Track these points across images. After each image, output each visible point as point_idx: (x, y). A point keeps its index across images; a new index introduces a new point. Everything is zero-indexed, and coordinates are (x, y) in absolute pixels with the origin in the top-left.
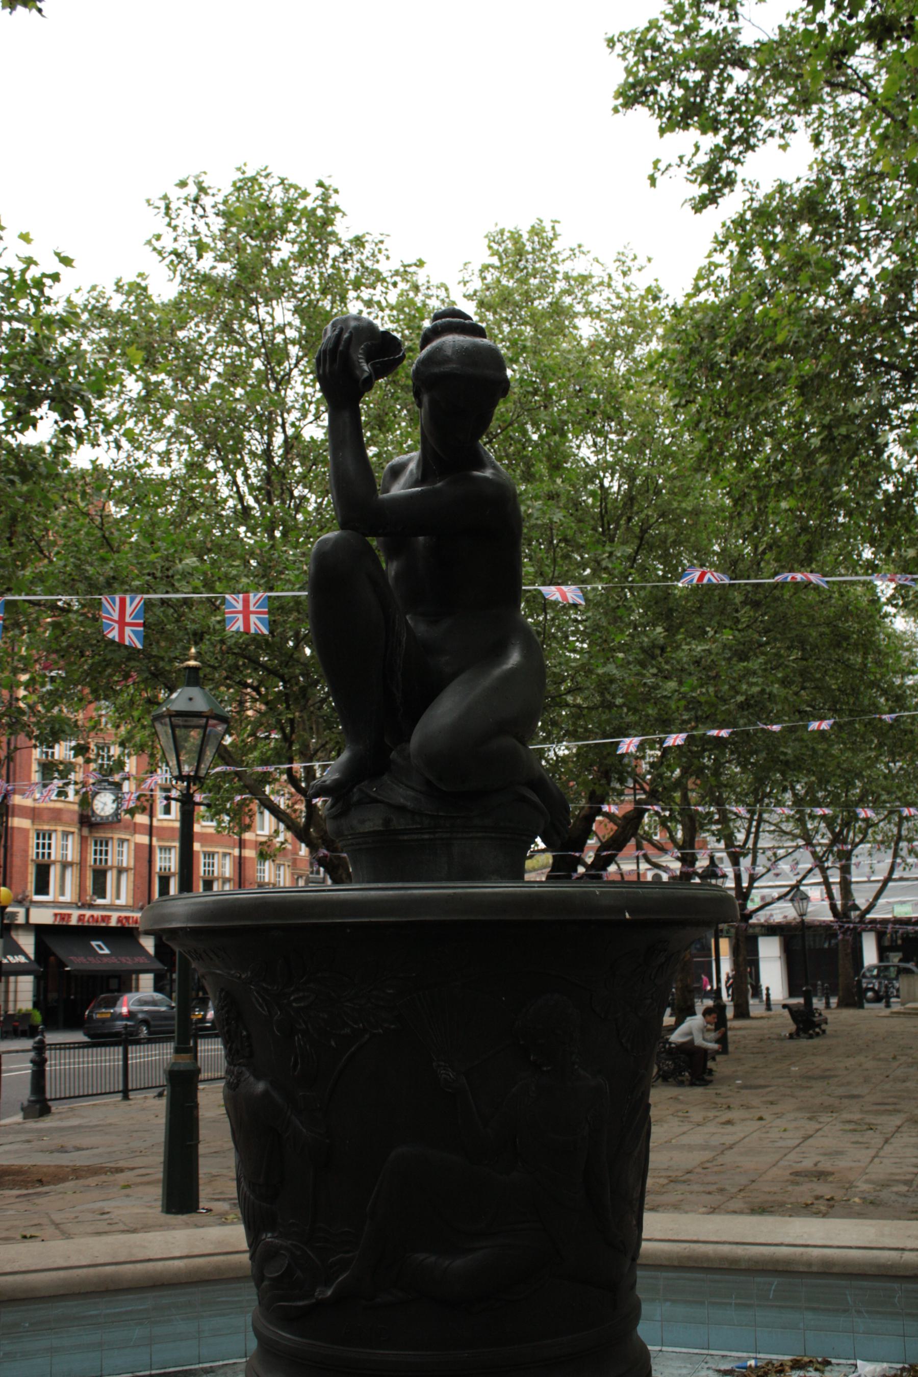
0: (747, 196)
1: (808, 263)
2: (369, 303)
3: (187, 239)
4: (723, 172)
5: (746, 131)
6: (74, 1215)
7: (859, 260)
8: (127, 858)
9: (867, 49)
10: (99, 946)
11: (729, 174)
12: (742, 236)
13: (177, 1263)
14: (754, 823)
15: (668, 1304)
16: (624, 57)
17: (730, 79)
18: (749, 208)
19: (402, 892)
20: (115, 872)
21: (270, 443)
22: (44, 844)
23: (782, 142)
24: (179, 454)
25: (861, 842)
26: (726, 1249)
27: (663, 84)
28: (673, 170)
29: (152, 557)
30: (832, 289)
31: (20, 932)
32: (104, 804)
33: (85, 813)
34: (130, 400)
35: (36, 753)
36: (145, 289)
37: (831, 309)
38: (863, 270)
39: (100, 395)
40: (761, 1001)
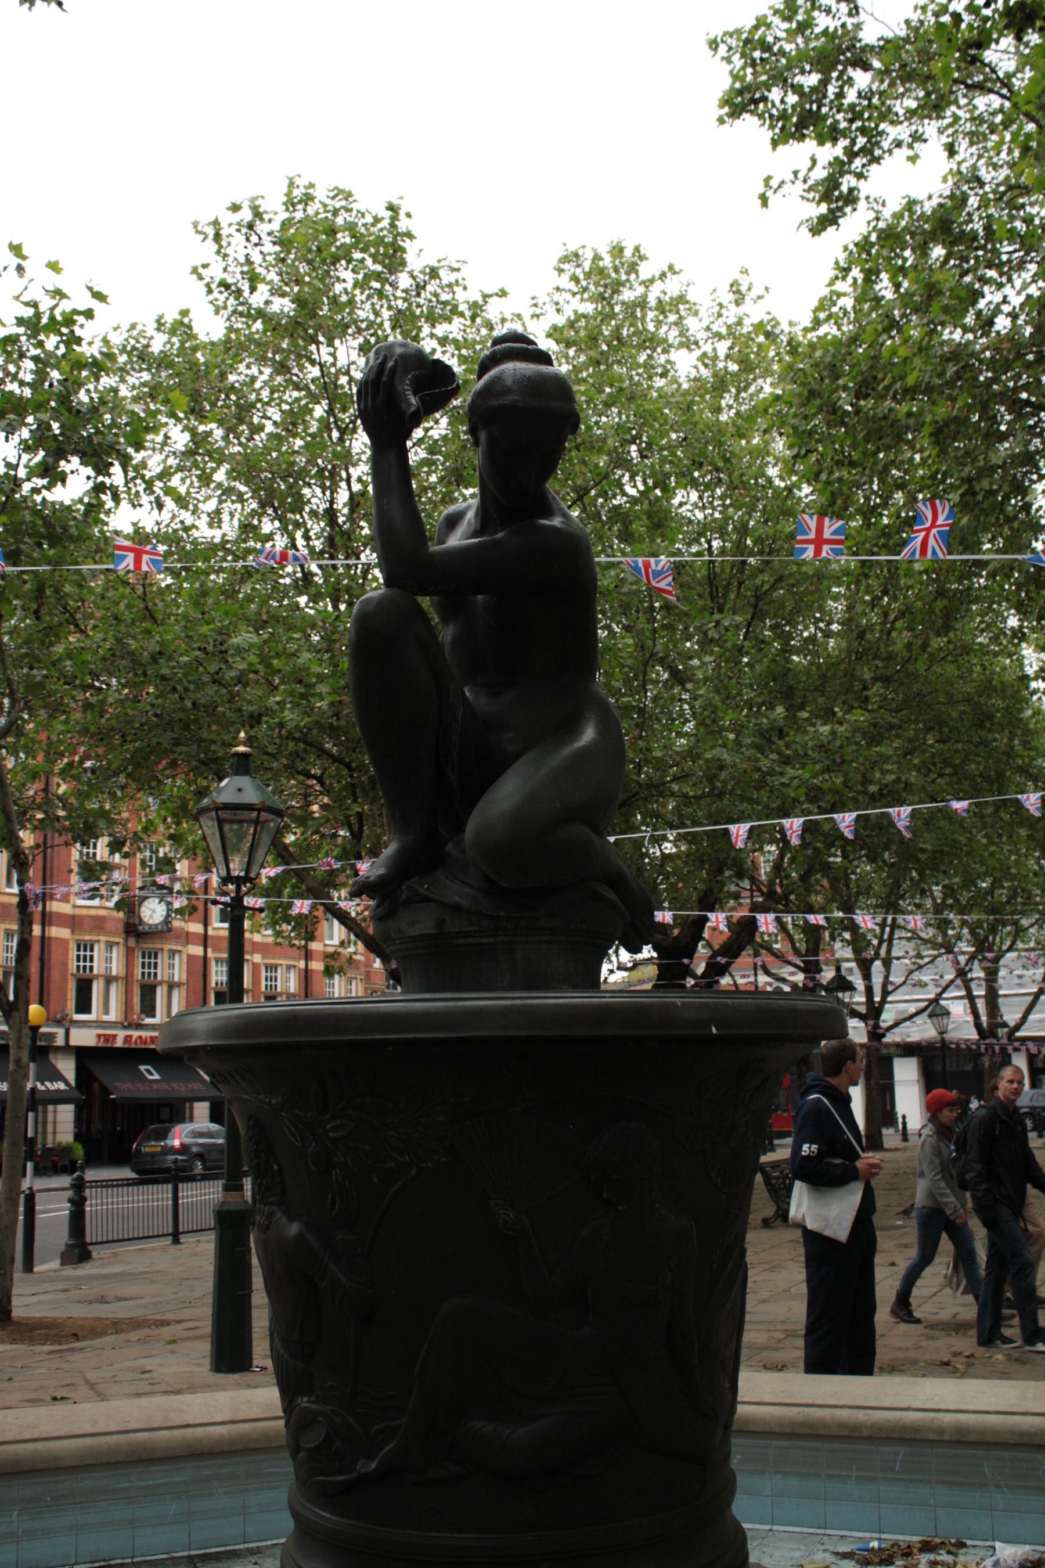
0: (872, 215)
1: (940, 293)
2: (443, 341)
3: (239, 269)
4: (844, 188)
5: (869, 141)
6: (110, 1374)
7: (1000, 286)
8: (179, 973)
9: (1007, 42)
10: (148, 1071)
11: (851, 190)
12: (867, 261)
13: (219, 1429)
14: (888, 929)
15: (779, 1476)
16: (728, 60)
17: (850, 81)
18: (874, 228)
19: (451, 1004)
20: (165, 987)
21: (332, 502)
22: (85, 957)
23: (911, 153)
24: (232, 515)
25: (1010, 949)
26: (845, 1413)
27: (775, 89)
28: (787, 188)
29: (205, 629)
30: (969, 319)
31: (60, 1056)
32: (153, 912)
33: (131, 921)
34: (174, 453)
35: (75, 853)
36: (190, 328)
37: (968, 343)
38: (1005, 297)
39: (139, 446)
40: (897, 1130)
